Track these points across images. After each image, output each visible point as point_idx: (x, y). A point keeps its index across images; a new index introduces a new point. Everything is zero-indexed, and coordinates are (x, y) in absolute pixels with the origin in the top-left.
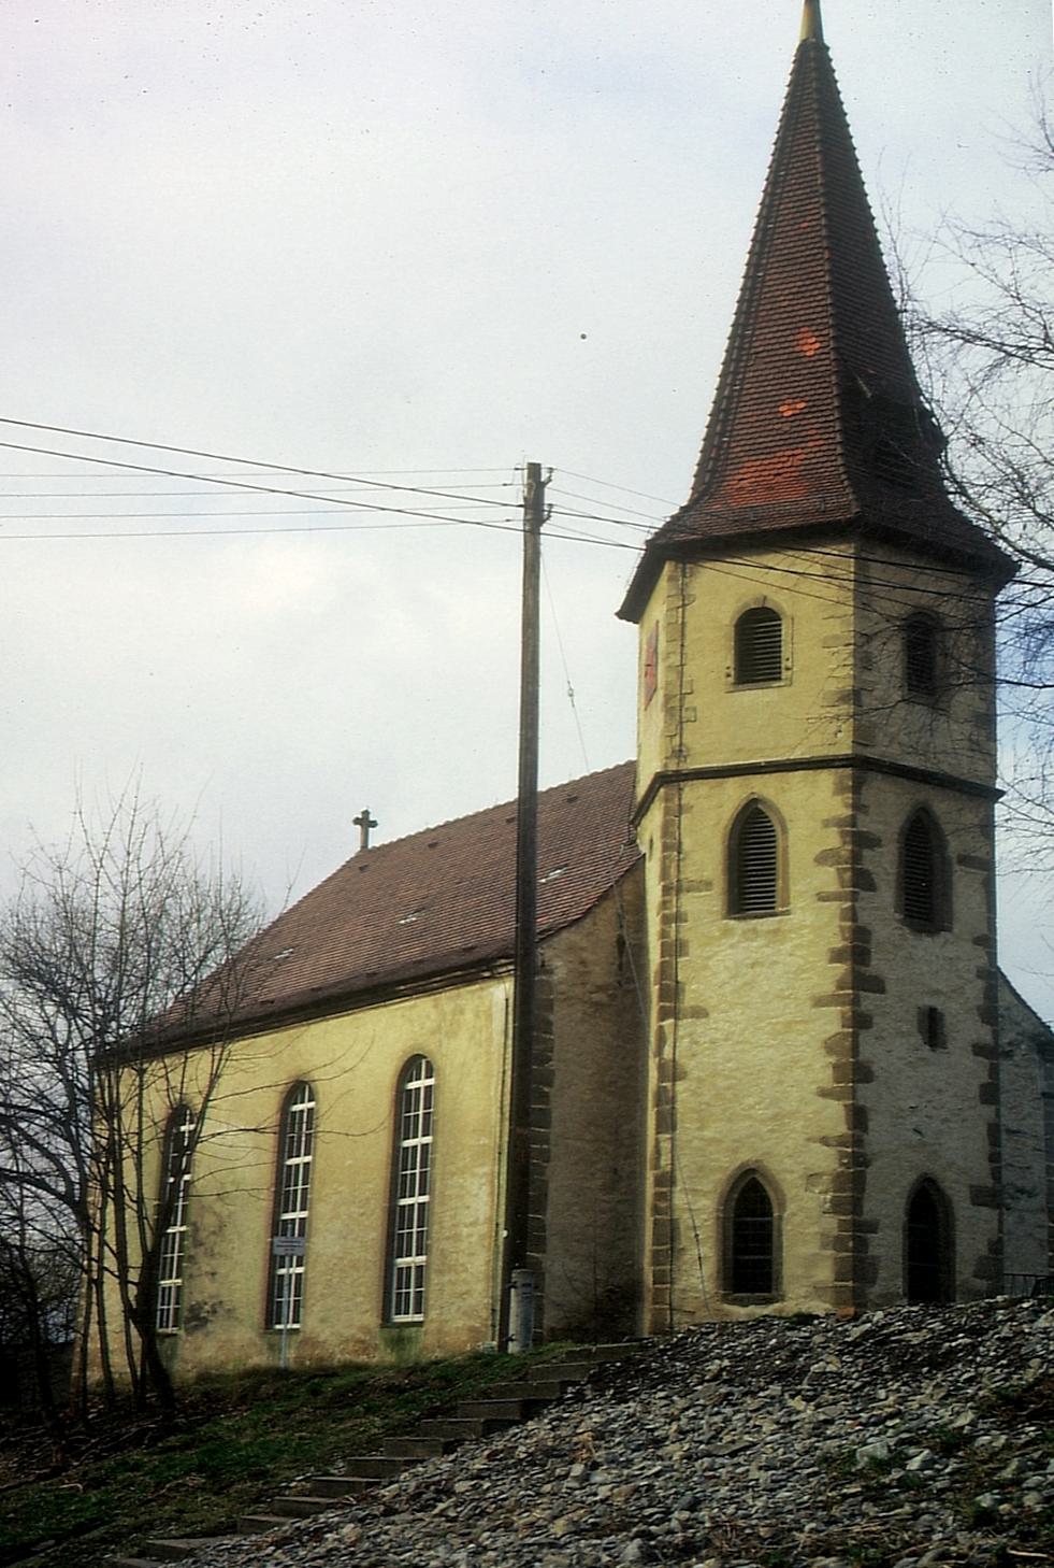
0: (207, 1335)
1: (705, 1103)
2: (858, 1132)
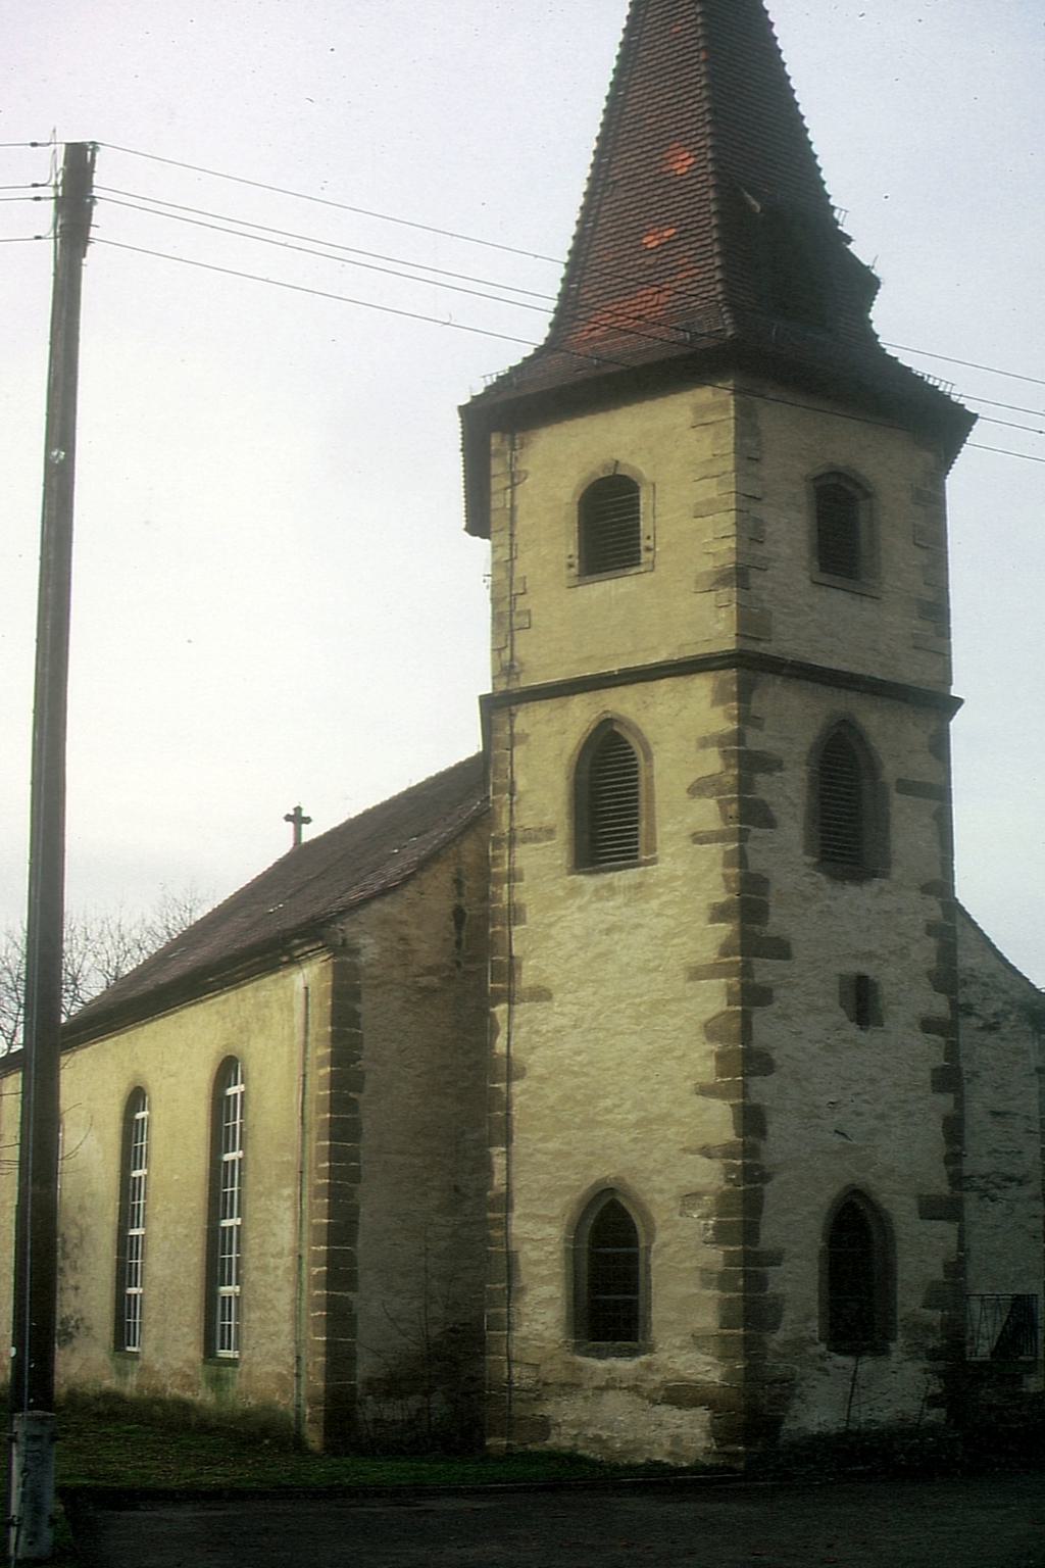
0: (73, 1350)
1: (547, 1107)
2: (751, 1139)
